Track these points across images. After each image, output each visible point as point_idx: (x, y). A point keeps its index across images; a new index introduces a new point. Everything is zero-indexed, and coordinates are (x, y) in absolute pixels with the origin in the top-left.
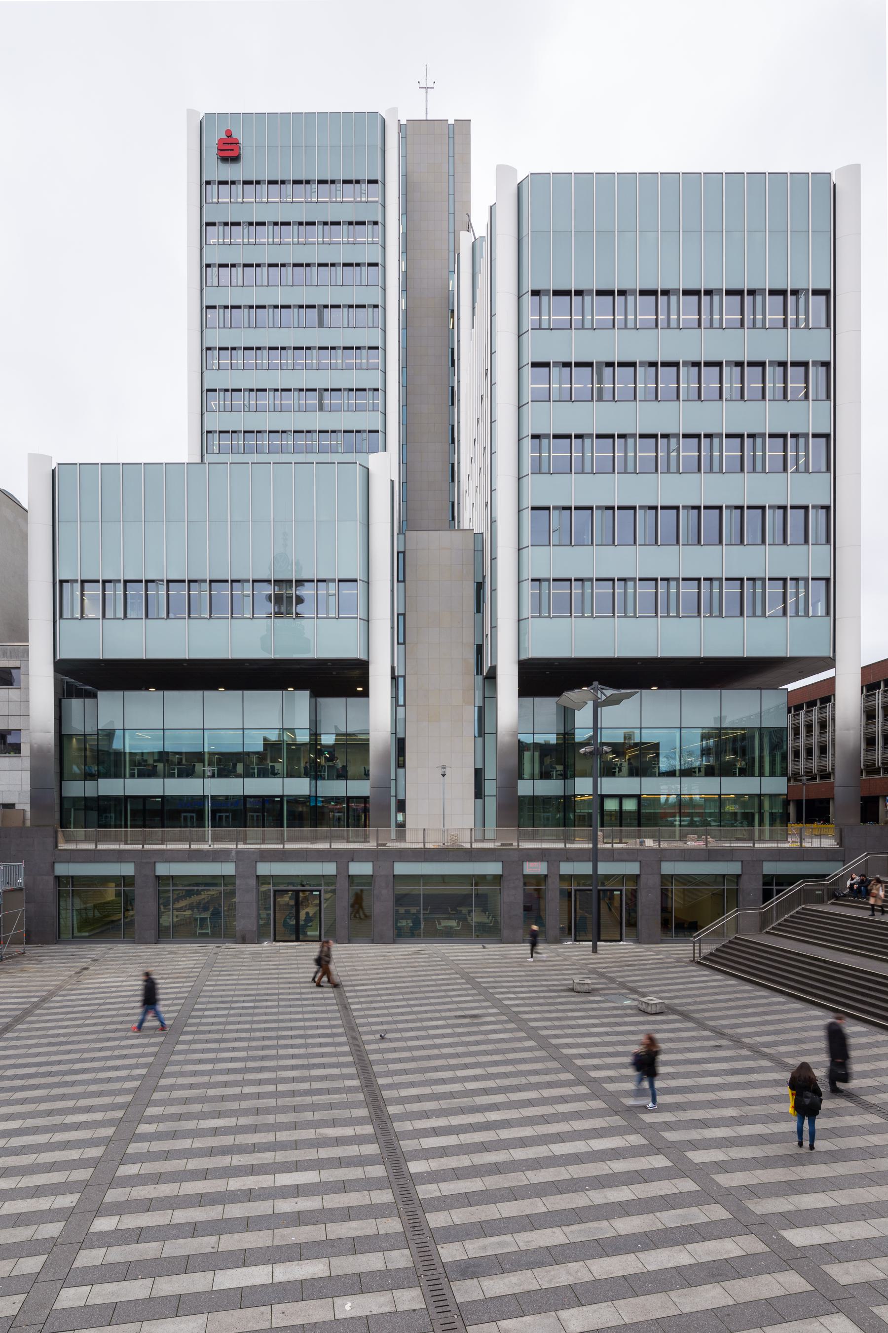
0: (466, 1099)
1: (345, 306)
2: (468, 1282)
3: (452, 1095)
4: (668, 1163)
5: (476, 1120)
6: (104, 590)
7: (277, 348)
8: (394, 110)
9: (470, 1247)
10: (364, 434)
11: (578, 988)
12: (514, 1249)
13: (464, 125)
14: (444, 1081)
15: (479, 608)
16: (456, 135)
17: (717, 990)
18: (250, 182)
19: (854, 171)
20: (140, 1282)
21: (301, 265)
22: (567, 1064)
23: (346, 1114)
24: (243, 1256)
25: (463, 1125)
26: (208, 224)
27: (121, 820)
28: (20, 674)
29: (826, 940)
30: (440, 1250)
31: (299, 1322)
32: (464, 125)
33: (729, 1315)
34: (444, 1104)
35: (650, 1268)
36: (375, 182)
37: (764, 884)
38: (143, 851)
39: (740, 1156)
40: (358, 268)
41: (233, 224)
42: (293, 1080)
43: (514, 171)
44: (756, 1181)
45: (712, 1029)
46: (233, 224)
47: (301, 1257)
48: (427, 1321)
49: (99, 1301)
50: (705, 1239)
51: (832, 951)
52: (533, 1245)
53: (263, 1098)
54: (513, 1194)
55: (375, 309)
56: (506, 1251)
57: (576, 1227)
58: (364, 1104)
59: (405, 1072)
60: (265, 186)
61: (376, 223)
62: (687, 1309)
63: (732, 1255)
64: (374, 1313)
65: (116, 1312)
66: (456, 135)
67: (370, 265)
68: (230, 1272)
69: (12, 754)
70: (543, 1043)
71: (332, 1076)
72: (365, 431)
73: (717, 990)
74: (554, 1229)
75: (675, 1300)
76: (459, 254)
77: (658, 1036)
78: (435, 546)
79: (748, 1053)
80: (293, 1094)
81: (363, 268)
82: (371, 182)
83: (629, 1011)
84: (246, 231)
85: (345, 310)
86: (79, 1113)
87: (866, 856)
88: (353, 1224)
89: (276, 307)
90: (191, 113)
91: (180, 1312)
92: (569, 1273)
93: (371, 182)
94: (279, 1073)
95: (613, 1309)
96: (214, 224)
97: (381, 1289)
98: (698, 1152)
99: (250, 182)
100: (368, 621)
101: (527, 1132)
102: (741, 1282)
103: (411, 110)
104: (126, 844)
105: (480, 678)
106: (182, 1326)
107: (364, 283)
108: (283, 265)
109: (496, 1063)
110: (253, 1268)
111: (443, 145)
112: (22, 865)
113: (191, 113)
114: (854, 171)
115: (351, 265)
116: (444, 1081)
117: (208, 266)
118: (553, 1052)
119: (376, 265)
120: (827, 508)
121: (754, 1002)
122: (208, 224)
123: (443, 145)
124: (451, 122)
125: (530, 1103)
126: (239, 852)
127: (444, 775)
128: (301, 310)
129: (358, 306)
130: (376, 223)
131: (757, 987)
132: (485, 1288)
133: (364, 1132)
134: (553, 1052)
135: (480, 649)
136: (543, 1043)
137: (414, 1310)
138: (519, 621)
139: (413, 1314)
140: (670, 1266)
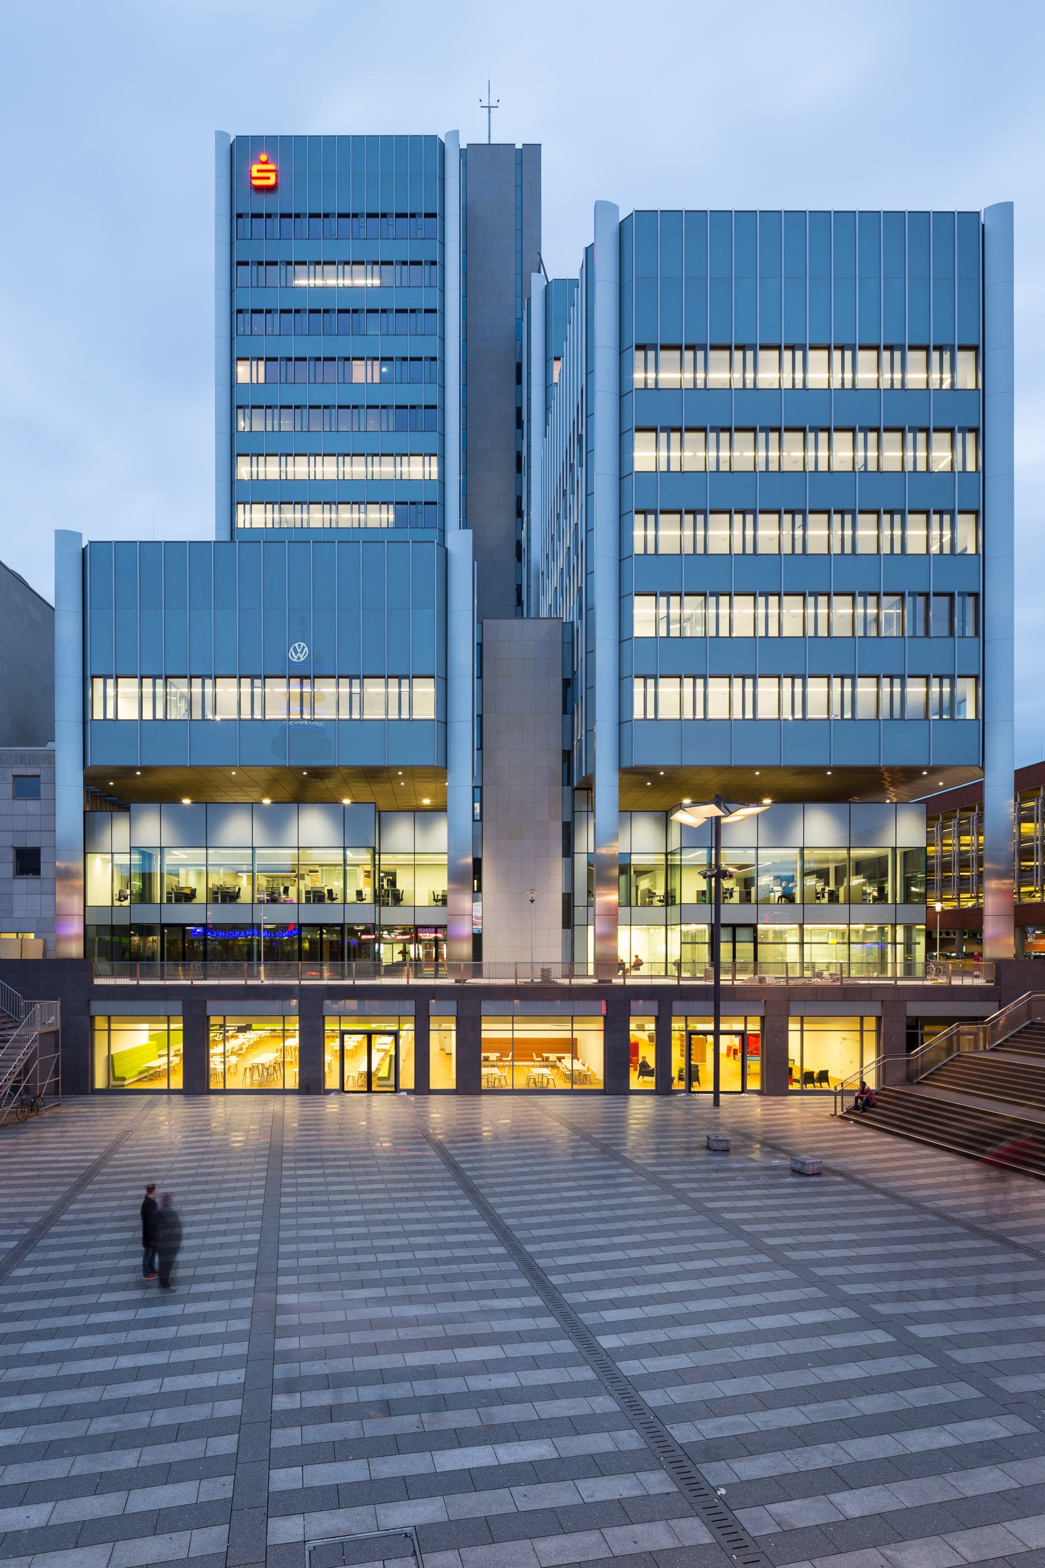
0: (634, 1269)
1: (340, 359)
2: (715, 1464)
3: (616, 1264)
4: (890, 1339)
5: (655, 1292)
6: (141, 685)
7: (319, 407)
8: (455, 134)
9: (703, 1427)
10: (419, 507)
11: (715, 1145)
12: (752, 1429)
13: (533, 150)
14: (601, 1249)
15: (567, 707)
16: (524, 161)
17: (874, 1148)
18: (260, 216)
19: (1006, 210)
20: (354, 1463)
21: (318, 311)
22: (734, 1230)
23: (504, 1284)
24: (454, 1436)
25: (642, 1296)
26: (239, 263)
28: (39, 783)
29: (993, 1092)
30: (672, 1432)
31: (546, 1505)
32: (533, 150)
33: (1018, 1498)
34: (613, 1273)
35: (913, 1450)
36: (434, 215)
37: (908, 1027)
38: (192, 987)
39: (968, 1330)
40: (384, 315)
41: (269, 263)
43: (614, 208)
44: (996, 1358)
45: (884, 1192)
46: (269, 263)
47: (519, 1438)
48: (686, 1504)
49: (316, 1483)
50: (962, 1419)
52: (773, 1426)
53: (404, 1267)
54: (730, 1371)
55: (433, 363)
56: (744, 1431)
57: (813, 1407)
58: (521, 1274)
59: (553, 1238)
60: (277, 221)
61: (434, 263)
62: (970, 1493)
63: (999, 1436)
64: (624, 1496)
65: (341, 1495)
66: (524, 161)
67: (427, 311)
68: (448, 1452)
69: (30, 875)
70: (698, 1207)
71: (471, 1242)
72: (420, 503)
73: (874, 1148)
74: (790, 1409)
75: (953, 1482)
76: (529, 300)
77: (154, 1292)
78: (522, 638)
79: (935, 1218)
80: (398, 1264)
81: (391, 315)
82: (428, 215)
83: (781, 1172)
84: (283, 270)
85: (312, 363)
86: (203, 1282)
87: (1029, 995)
88: (563, 1403)
89: (318, 359)
90: (220, 135)
92: (824, 1455)
93: (428, 215)
94: (411, 1239)
95: (887, 1493)
96: (246, 263)
97: (622, 1471)
98: (920, 1327)
99: (260, 216)
100: (446, 723)
101: (717, 1304)
102: (1019, 1464)
103: (473, 134)
104: (162, 979)
105: (568, 789)
106: (420, 1509)
107: (419, 332)
108: (269, 311)
109: (653, 1229)
110: (472, 1449)
111: (510, 175)
112: (58, 1003)
113: (220, 135)
114: (1006, 210)
115: (405, 311)
116: (601, 1249)
117: (240, 311)
118: (714, 1218)
119: (434, 311)
120: (976, 595)
121: (922, 1161)
122: (239, 263)
123: (510, 175)
124: (519, 146)
125: (708, 1273)
126: (302, 988)
127: (532, 901)
128: (318, 363)
129: (326, 359)
130: (434, 263)
131: (919, 1145)
132: (737, 1471)
133: (533, 1304)
134: (714, 1218)
135: (567, 756)
136: (698, 1207)
137: (668, 1494)
138: (620, 723)
139: (667, 1498)
140: (934, 1447)
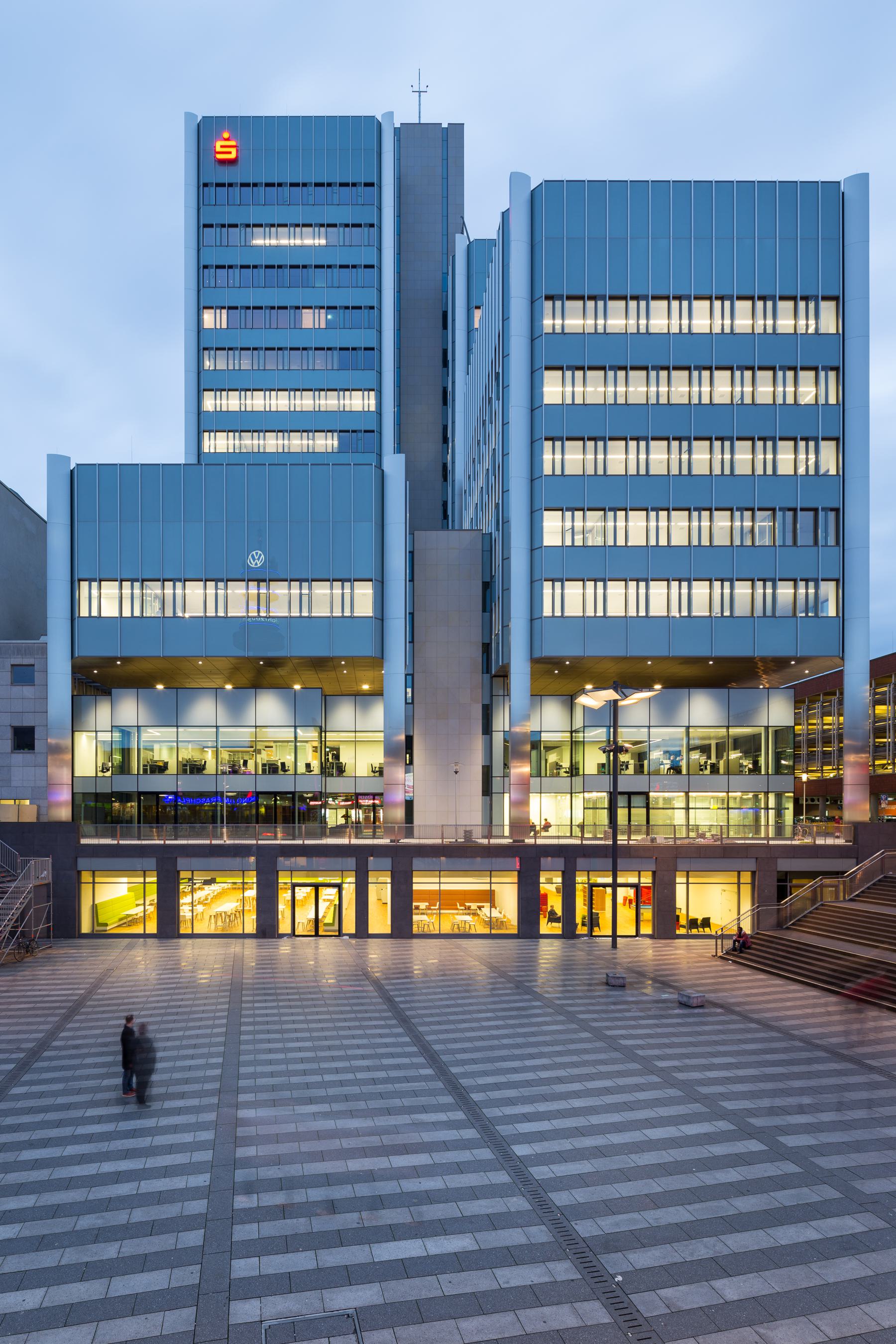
0: (543, 1088)
1: (291, 307)
2: (613, 1255)
3: (528, 1083)
4: (763, 1147)
5: (562, 1107)
6: (121, 587)
7: (273, 349)
8: (390, 115)
9: (603, 1223)
10: (360, 434)
11: (613, 982)
12: (644, 1225)
13: (457, 129)
14: (515, 1070)
15: (487, 606)
16: (450, 138)
17: (749, 984)
18: (223, 185)
19: (862, 180)
20: (304, 1254)
21: (273, 267)
22: (629, 1054)
23: (432, 1101)
24: (390, 1231)
25: (550, 1111)
26: (205, 226)
27: (299, 809)
28: (34, 671)
29: (852, 936)
30: (576, 1227)
31: (468, 1290)
32: (457, 129)
33: (873, 1284)
34: (525, 1091)
35: (783, 1243)
36: (372, 185)
37: (779, 881)
38: (165, 846)
39: (830, 1140)
40: (329, 270)
41: (230, 226)
42: (305, 1073)
43: (527, 178)
44: (854, 1164)
45: (758, 1022)
46: (230, 226)
47: (445, 1233)
48: (588, 1289)
49: (271, 1271)
50: (825, 1217)
51: (869, 948)
52: (663, 1222)
53: (346, 1086)
54: (626, 1175)
55: (371, 311)
56: (638, 1227)
57: (697, 1206)
58: (446, 1092)
59: (474, 1061)
60: (237, 189)
61: (372, 225)
62: (831, 1280)
63: (856, 1231)
64: (535, 1282)
65: (292, 1281)
66: (450, 138)
67: (366, 267)
68: (384, 1245)
69: (26, 750)
70: (598, 1034)
71: (404, 1065)
72: (360, 431)
73: (749, 984)
74: (677, 1208)
75: (817, 1270)
76: (454, 257)
78: (448, 547)
79: (801, 1044)
80: (342, 1083)
81: (335, 270)
82: (367, 185)
83: (670, 1005)
84: (243, 232)
85: (268, 311)
86: (174, 1099)
87: (883, 853)
88: (483, 1202)
89: (273, 308)
90: (189, 116)
91: (135, 1312)
92: (706, 1247)
93: (367, 185)
94: (352, 1062)
95: (761, 1279)
96: (211, 226)
97: (533, 1261)
98: (789, 1137)
99: (223, 185)
100: (382, 620)
101: (615, 1118)
102: (874, 1255)
103: (406, 115)
104: (139, 839)
105: (487, 676)
106: (360, 1293)
107: (360, 285)
108: (230, 267)
109: (560, 1054)
110: (405, 1242)
111: (437, 150)
112: (50, 860)
113: (189, 116)
114: (862, 180)
115: (347, 267)
116: (515, 1070)
117: (205, 267)
118: (612, 1044)
119: (372, 267)
120: (837, 510)
121: (790, 995)
122: (205, 226)
123: (437, 150)
124: (445, 125)
125: (607, 1091)
126: (259, 847)
127: (456, 772)
128: (272, 311)
129: (279, 308)
130: (372, 225)
131: (788, 982)
132: (632, 1261)
133: (457, 1118)
134: (612, 1044)
135: (486, 648)
136: (598, 1034)
137: (572, 1280)
138: (531, 620)
139: (572, 1284)
140: (801, 1240)
